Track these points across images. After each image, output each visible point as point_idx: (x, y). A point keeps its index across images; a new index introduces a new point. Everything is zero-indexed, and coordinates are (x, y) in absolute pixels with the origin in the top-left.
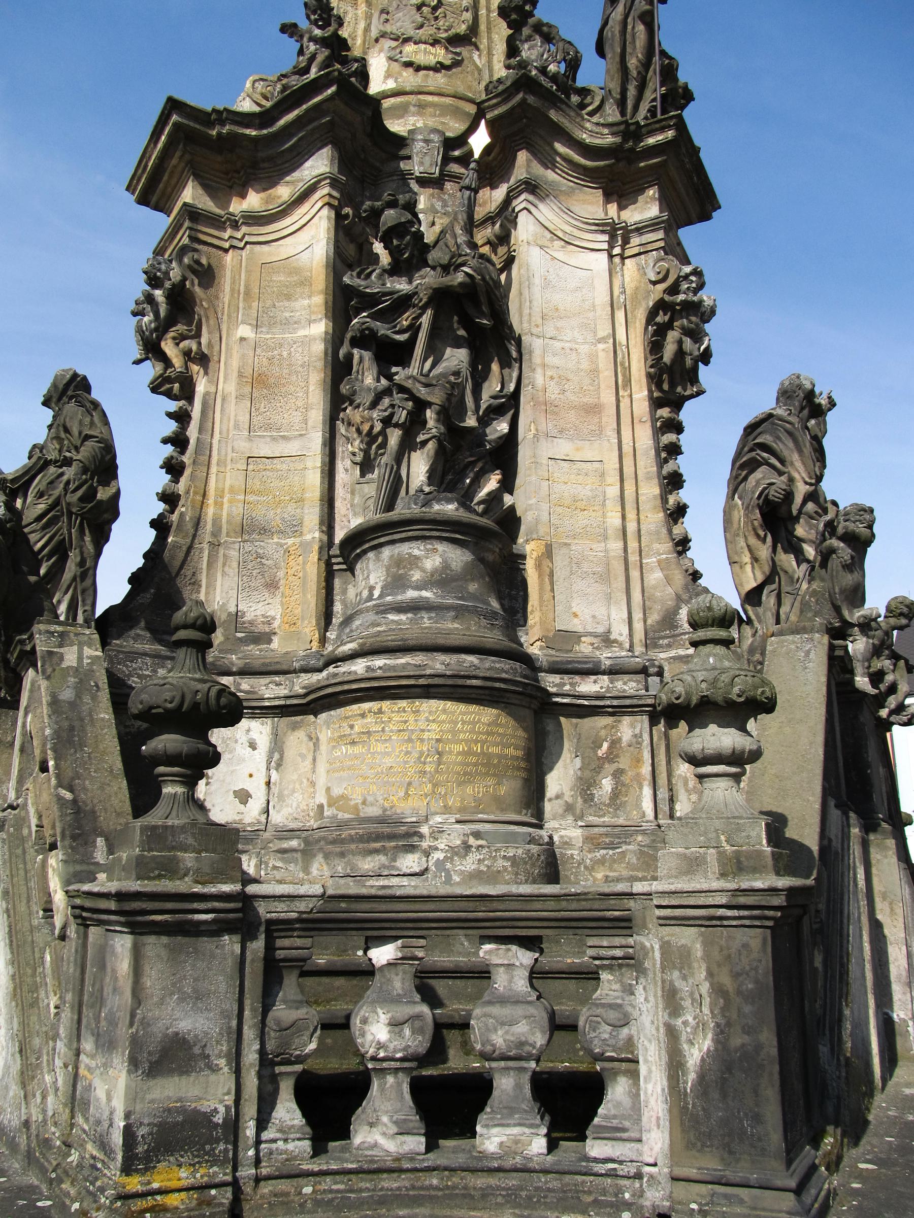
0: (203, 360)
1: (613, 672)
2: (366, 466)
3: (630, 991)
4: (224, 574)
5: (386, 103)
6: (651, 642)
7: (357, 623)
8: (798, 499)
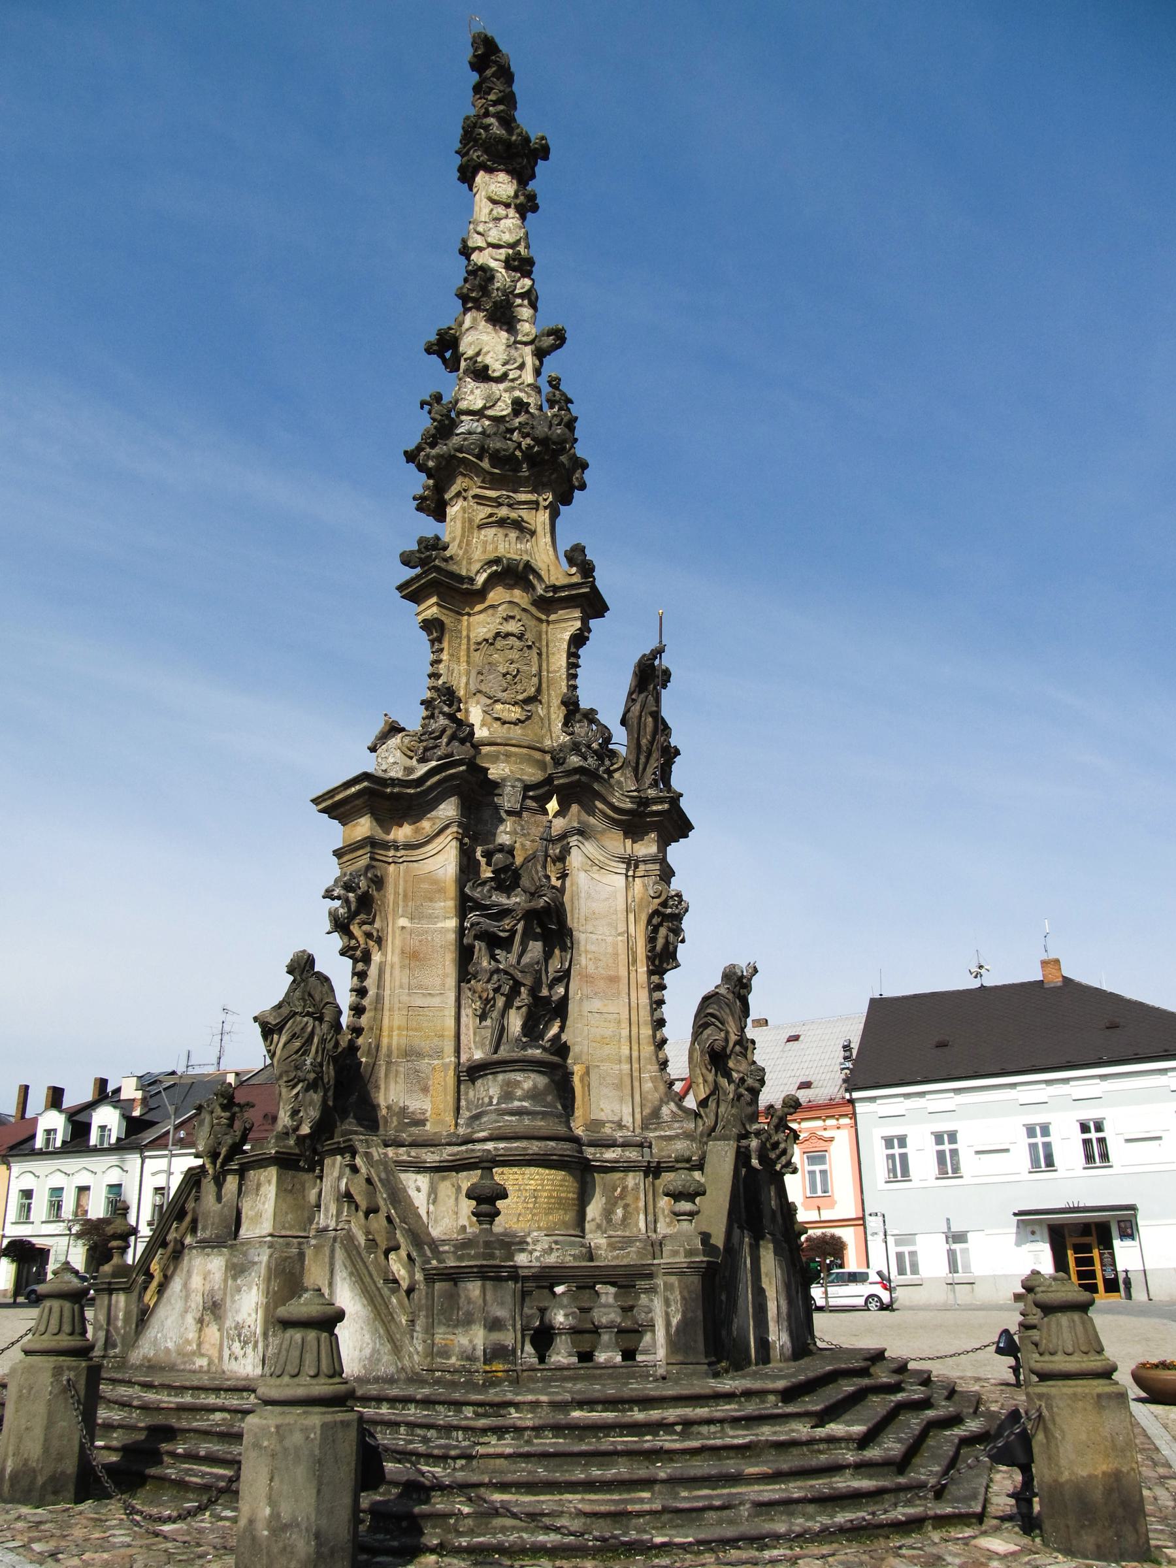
0: (379, 941)
1: (625, 1145)
2: (483, 1017)
3: (652, 1300)
4: (396, 1082)
5: (485, 750)
6: (645, 1127)
7: (484, 1119)
8: (731, 1044)
